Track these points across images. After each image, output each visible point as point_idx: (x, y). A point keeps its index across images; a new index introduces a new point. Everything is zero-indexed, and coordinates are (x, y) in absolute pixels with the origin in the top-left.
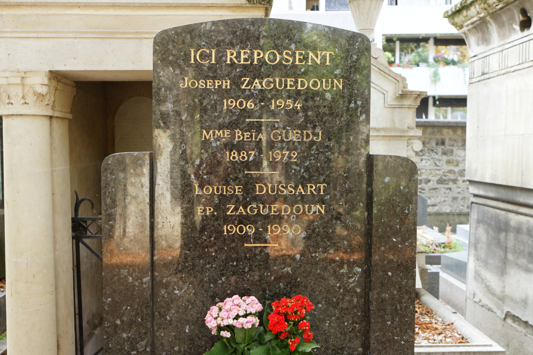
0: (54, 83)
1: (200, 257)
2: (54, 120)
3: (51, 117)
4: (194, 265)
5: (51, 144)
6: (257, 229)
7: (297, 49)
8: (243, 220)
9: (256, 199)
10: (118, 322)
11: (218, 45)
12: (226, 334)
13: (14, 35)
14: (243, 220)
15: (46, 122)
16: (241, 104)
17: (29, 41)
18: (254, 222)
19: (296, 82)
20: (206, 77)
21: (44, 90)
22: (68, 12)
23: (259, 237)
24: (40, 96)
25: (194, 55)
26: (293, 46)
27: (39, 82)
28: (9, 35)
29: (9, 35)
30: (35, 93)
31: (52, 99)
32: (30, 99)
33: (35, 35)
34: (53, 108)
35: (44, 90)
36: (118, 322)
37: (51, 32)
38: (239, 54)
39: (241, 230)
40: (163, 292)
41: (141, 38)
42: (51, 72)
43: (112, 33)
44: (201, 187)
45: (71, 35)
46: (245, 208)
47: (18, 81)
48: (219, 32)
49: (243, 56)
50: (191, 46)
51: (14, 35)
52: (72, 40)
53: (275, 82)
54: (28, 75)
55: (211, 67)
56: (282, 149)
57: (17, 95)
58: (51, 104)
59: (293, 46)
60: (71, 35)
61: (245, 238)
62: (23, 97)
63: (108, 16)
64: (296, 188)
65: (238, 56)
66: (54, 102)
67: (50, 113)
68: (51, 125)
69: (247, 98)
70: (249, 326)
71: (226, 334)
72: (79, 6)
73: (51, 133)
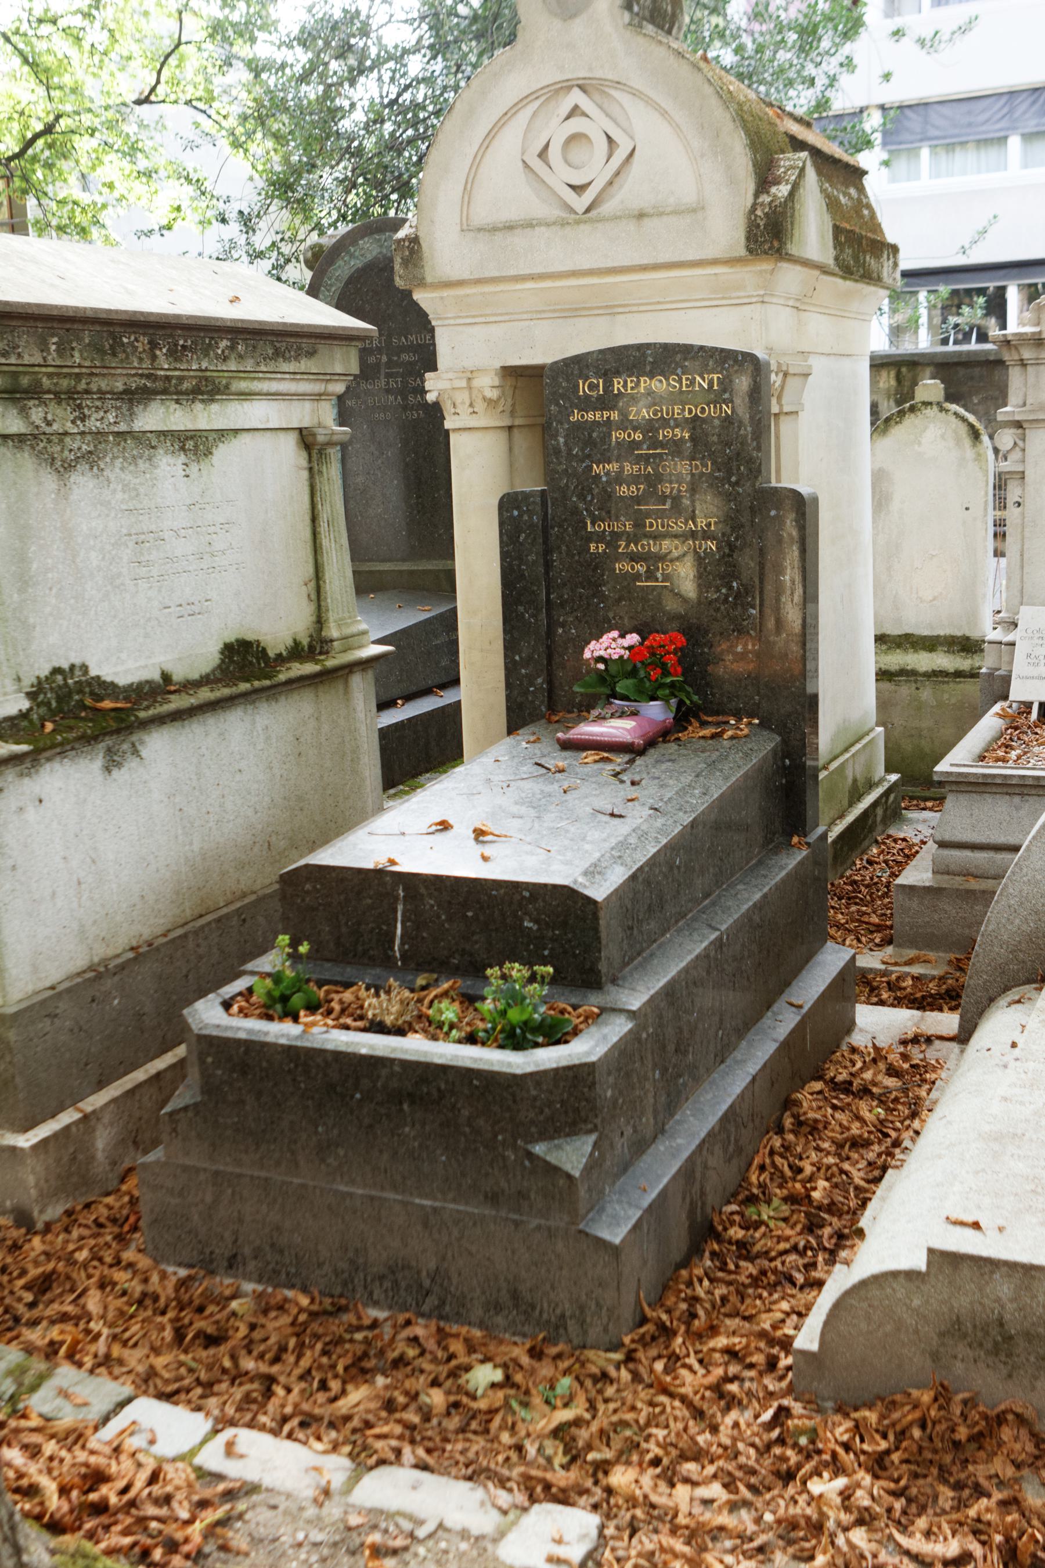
0: (510, 382)
1: (594, 596)
2: (515, 430)
3: (510, 428)
4: (588, 604)
5: (511, 465)
6: (648, 568)
7: (684, 373)
8: (634, 558)
9: (647, 536)
10: (517, 658)
11: (605, 374)
12: (601, 666)
13: (459, 321)
14: (634, 558)
15: (503, 436)
16: (629, 435)
17: (476, 328)
18: (645, 560)
19: (683, 410)
20: (595, 409)
21: (493, 394)
22: (519, 286)
23: (650, 575)
24: (490, 403)
25: (583, 388)
26: (679, 371)
27: (488, 384)
28: (452, 322)
29: (452, 322)
30: (484, 398)
31: (510, 401)
32: (480, 406)
33: (482, 320)
34: (512, 413)
35: (493, 394)
36: (517, 658)
37: (501, 314)
38: (625, 382)
39: (633, 568)
40: (560, 631)
41: (614, 314)
42: (504, 369)
43: (576, 309)
44: (593, 524)
45: (525, 316)
46: (636, 545)
47: (463, 383)
48: (605, 360)
49: (629, 385)
50: (580, 377)
51: (459, 321)
52: (527, 323)
53: (662, 411)
54: (475, 375)
55: (600, 398)
56: (671, 483)
57: (463, 403)
58: (508, 408)
59: (679, 371)
60: (525, 316)
61: (637, 577)
62: (471, 405)
63: (569, 287)
64: (686, 524)
65: (625, 386)
66: (513, 405)
67: (507, 422)
68: (510, 439)
69: (635, 429)
70: (616, 657)
71: (601, 666)
72: (532, 277)
73: (511, 449)
